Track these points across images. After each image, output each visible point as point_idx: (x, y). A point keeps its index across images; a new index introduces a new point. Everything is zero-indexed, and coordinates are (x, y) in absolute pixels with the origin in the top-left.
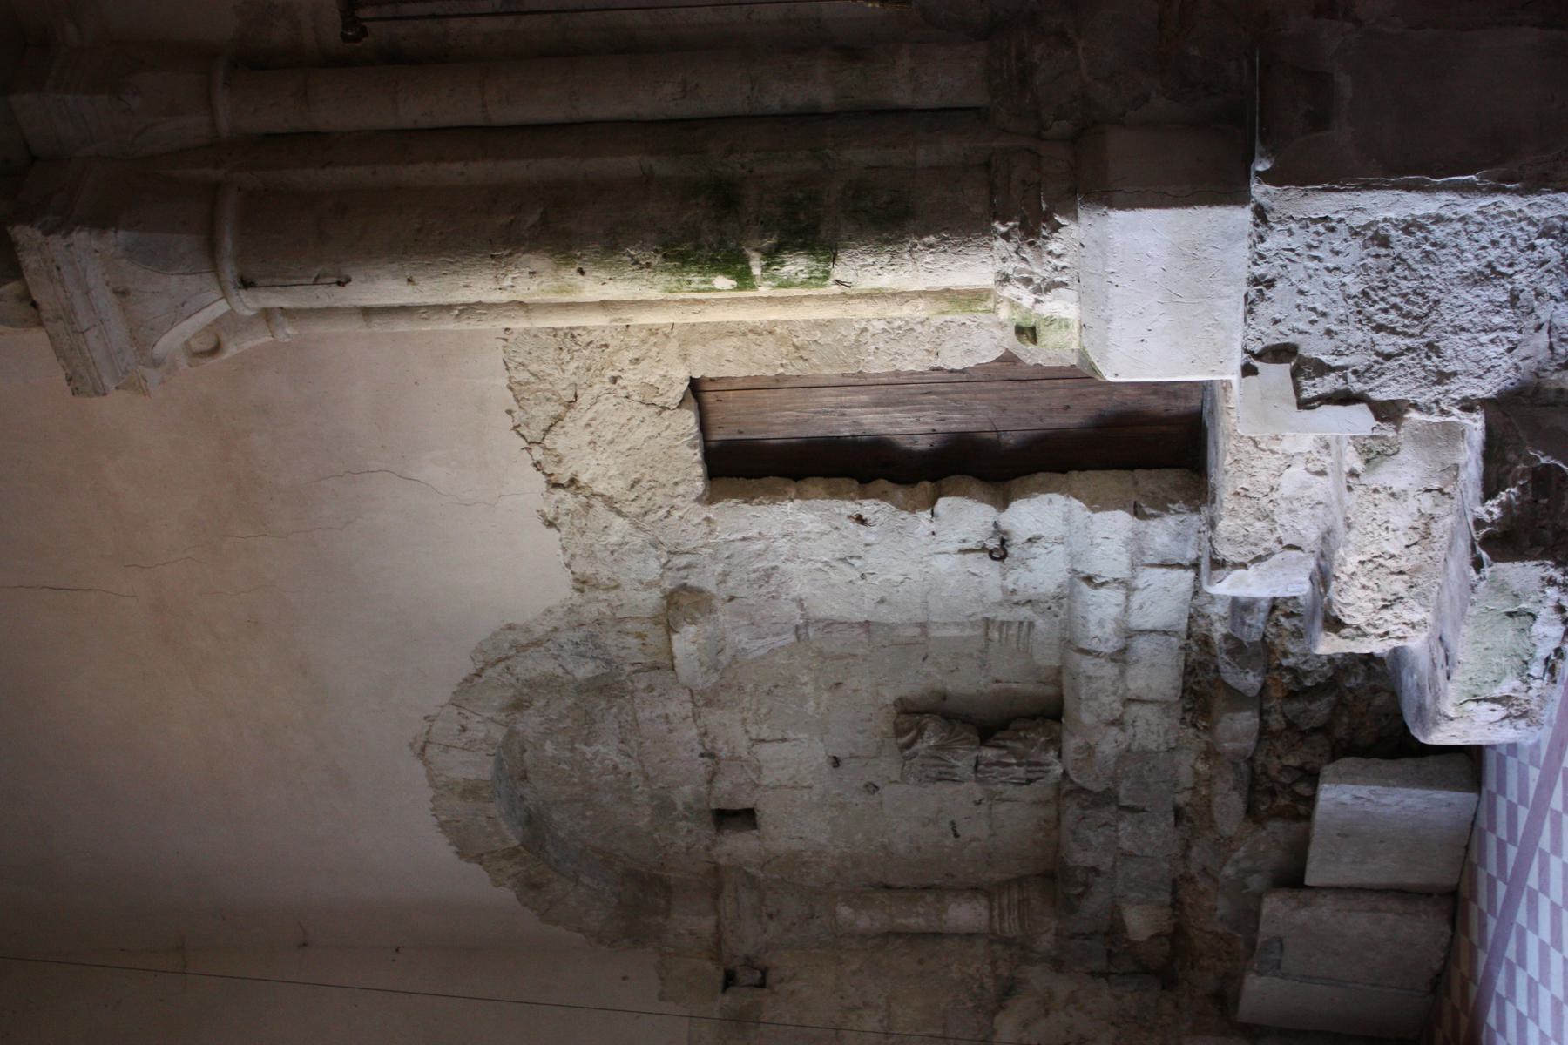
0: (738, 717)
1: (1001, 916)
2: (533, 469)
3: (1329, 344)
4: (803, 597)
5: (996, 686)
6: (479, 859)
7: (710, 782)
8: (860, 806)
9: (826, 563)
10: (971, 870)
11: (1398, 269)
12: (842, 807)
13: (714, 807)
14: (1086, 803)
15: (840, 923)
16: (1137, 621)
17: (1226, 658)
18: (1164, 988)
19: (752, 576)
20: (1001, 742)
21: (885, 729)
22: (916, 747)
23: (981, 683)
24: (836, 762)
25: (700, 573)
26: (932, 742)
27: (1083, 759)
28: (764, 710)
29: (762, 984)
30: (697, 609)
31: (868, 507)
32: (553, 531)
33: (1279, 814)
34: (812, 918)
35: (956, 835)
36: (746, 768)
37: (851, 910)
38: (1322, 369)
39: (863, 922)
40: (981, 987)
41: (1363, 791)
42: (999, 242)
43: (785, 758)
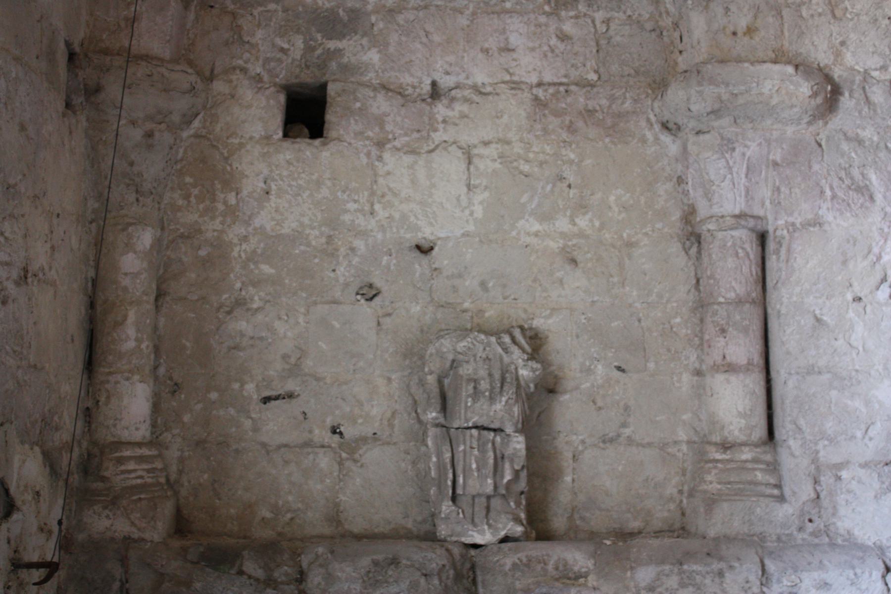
0: (512, 135)
1: (141, 459)
4: (826, 227)
5: (569, 455)
7: (385, 87)
8: (332, 275)
9: (879, 258)
10: (186, 418)
12: (329, 252)
13: (332, 89)
14: (444, 578)
15: (130, 229)
19: (856, 172)
21: (487, 315)
23: (574, 437)
24: (424, 250)
25: (860, 112)
27: (545, 570)
28: (525, 168)
34: (137, 192)
35: (266, 400)
36: (416, 135)
37: (148, 247)
43: (433, 186)
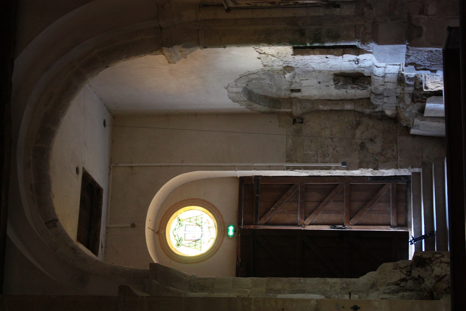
2: (256, 52)
3: (422, 63)
6: (237, 102)
7: (290, 85)
11: (435, 55)
13: (291, 89)
16: (387, 72)
17: (407, 80)
18: (394, 123)
20: (357, 83)
22: (338, 85)
26: (342, 83)
29: (302, 122)
30: (291, 71)
31: (328, 56)
32: (260, 60)
33: (419, 102)
35: (347, 92)
38: (420, 66)
39: (325, 108)
40: (353, 123)
41: (436, 104)
42: (357, 42)
